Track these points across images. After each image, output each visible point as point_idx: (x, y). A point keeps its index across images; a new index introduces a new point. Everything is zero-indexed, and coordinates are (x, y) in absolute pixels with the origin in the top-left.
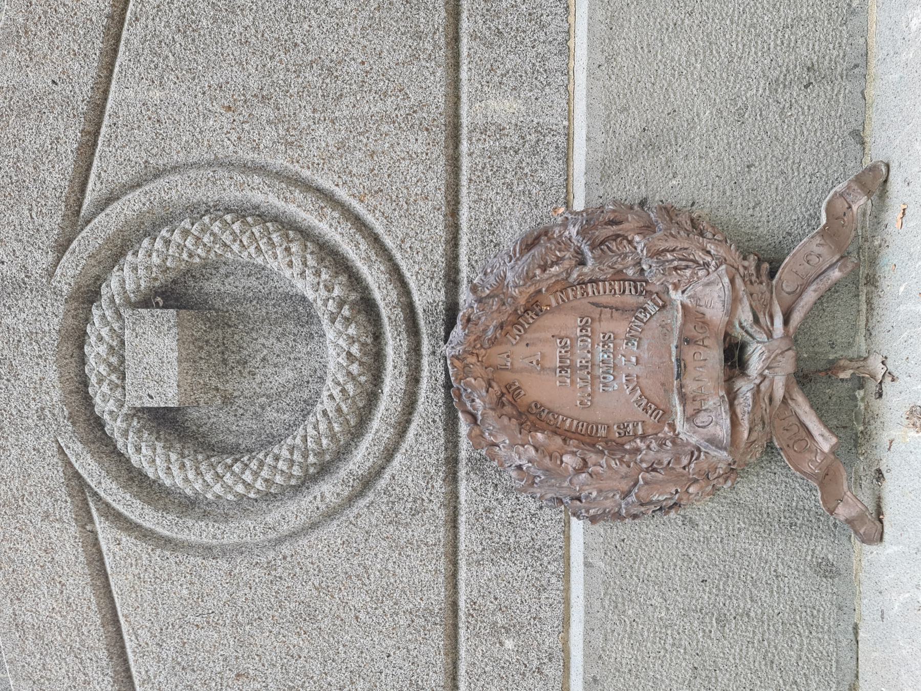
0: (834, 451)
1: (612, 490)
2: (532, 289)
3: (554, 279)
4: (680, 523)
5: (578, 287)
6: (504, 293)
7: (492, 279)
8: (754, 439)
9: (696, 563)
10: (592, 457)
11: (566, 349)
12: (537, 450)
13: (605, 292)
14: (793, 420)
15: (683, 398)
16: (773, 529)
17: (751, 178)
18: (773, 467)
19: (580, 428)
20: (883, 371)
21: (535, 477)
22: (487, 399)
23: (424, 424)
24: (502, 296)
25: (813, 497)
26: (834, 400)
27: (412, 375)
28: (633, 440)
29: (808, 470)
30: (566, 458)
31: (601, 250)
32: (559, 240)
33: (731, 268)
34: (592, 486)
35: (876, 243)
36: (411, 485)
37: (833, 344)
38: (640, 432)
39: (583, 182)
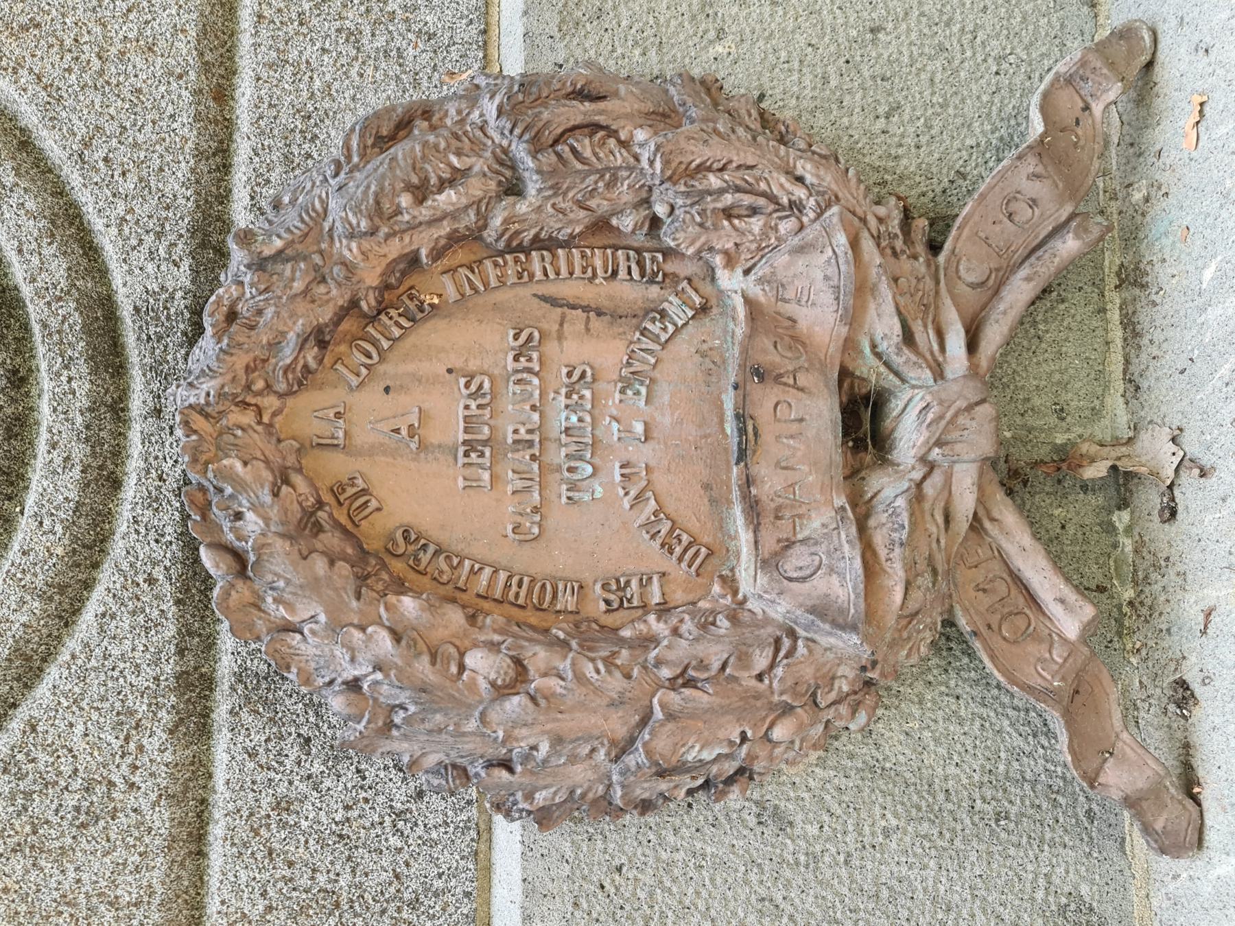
0: (1088, 632)
1: (588, 738)
2: (395, 249)
3: (445, 228)
4: (752, 821)
5: (508, 257)
6: (321, 252)
7: (291, 217)
8: (917, 606)
9: (791, 917)
10: (538, 656)
11: (480, 401)
12: (397, 637)
13: (571, 274)
14: (996, 567)
15: (753, 509)
16: (959, 827)
17: (880, 56)
18: (952, 683)
19: (514, 588)
20: (1176, 460)
21: (393, 708)
22: (274, 513)
23: (124, 587)
24: (317, 259)
25: (1041, 751)
26: (1072, 532)
27: (101, 468)
28: (639, 619)
29: (1036, 682)
30: (474, 659)
31: (558, 155)
32: (456, 129)
33: (850, 216)
34: (537, 729)
35: (1137, 196)
36: (79, 744)
37: (1062, 410)
38: (656, 598)
39: (520, 31)
